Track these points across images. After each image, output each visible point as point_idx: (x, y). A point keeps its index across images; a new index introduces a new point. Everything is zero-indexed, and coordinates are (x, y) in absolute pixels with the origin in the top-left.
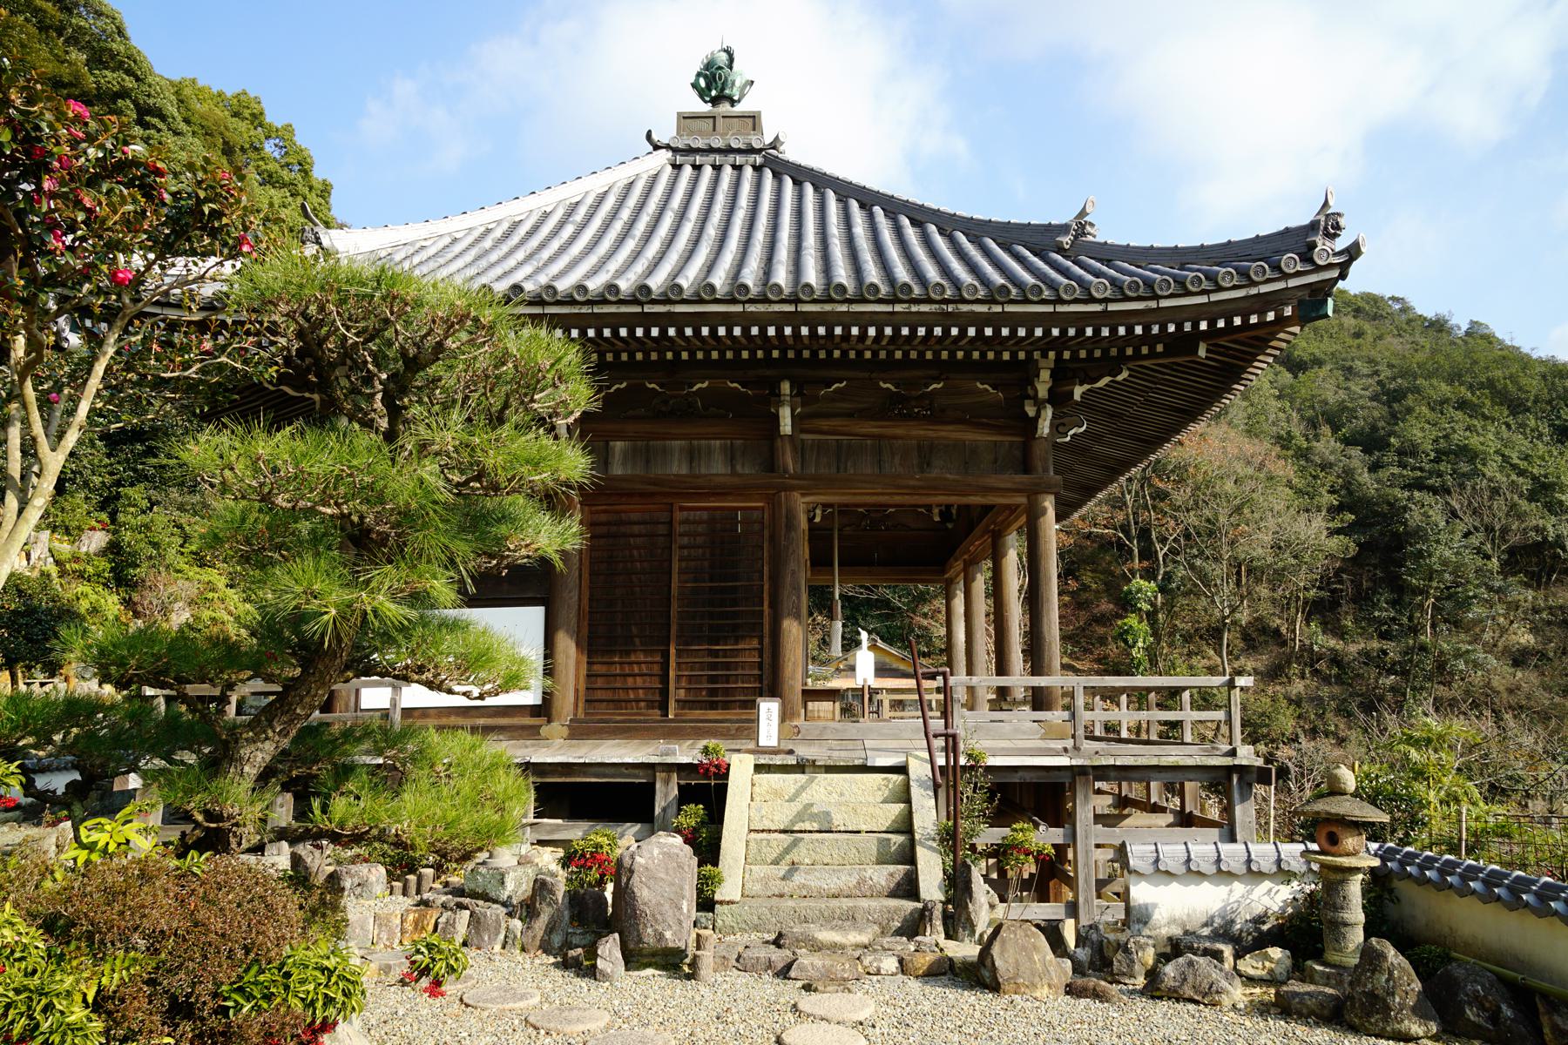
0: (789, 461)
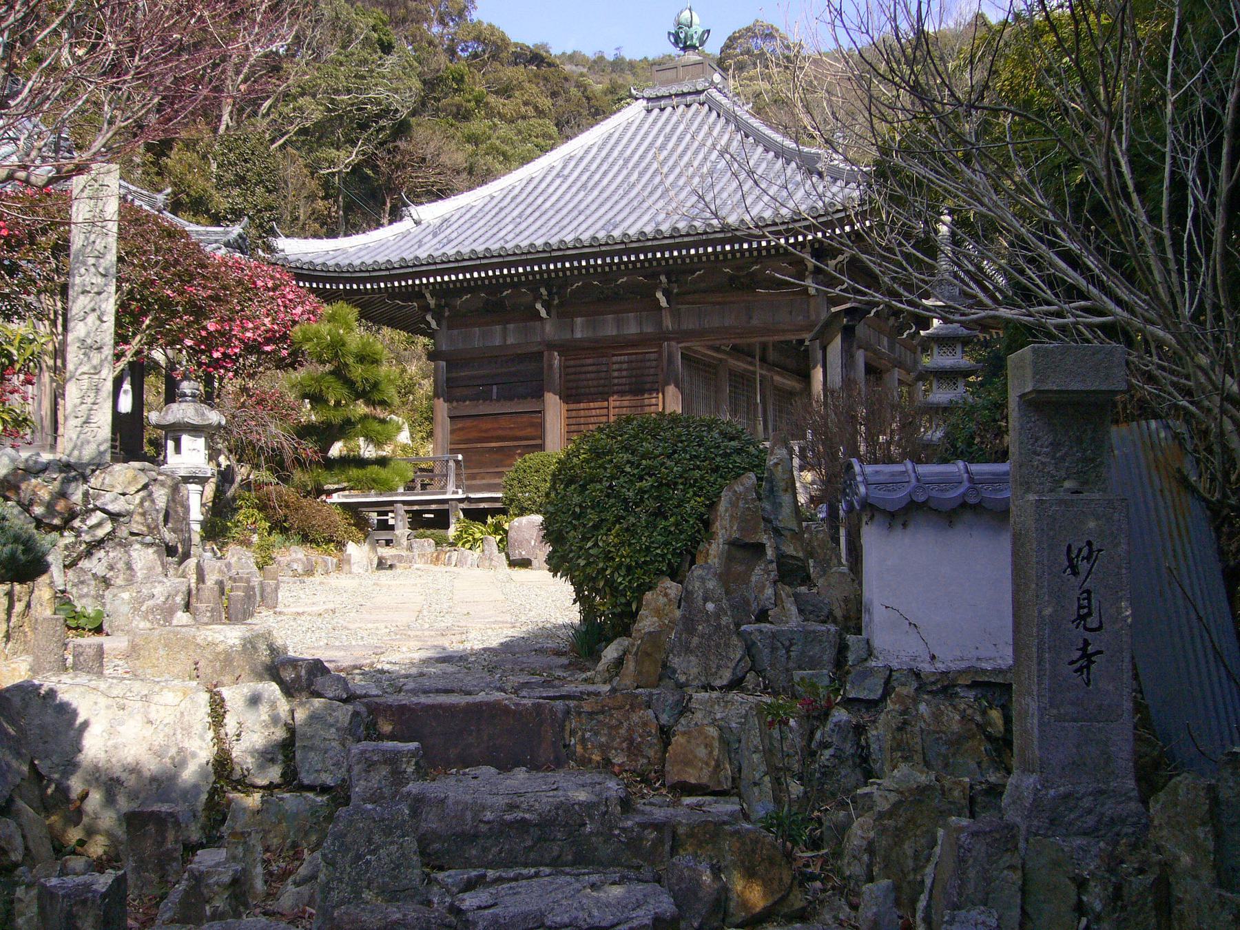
0: (668, 323)
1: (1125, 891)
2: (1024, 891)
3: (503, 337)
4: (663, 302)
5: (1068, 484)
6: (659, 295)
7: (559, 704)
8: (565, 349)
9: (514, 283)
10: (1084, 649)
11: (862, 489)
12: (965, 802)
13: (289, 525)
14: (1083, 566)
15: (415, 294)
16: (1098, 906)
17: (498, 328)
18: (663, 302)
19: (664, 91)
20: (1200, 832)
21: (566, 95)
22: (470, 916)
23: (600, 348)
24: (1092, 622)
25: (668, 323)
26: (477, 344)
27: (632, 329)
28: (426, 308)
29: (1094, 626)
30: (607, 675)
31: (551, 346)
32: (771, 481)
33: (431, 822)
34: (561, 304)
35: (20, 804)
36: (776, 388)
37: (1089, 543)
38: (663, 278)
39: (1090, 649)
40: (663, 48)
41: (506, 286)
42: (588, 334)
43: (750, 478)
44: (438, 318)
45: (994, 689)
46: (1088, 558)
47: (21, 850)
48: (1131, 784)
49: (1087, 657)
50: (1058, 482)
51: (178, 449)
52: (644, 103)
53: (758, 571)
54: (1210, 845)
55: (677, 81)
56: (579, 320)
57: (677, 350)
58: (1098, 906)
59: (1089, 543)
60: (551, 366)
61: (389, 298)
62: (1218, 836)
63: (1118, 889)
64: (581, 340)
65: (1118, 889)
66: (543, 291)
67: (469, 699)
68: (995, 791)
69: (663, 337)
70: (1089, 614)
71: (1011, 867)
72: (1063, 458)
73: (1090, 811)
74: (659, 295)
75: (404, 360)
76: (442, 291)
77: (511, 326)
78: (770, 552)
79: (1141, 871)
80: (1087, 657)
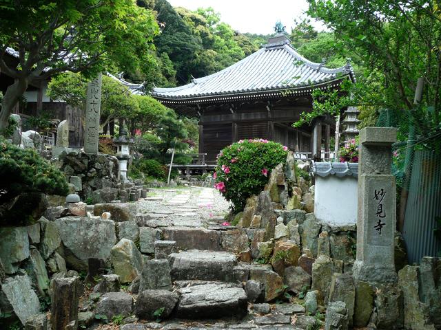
0: (270, 116)
1: (389, 300)
2: (356, 297)
3: (219, 118)
4: (268, 109)
5: (376, 171)
6: (267, 107)
7: (219, 232)
8: (240, 123)
9: (224, 103)
10: (379, 223)
11: (314, 170)
12: (341, 268)
13: (153, 173)
14: (380, 197)
15: (194, 105)
16: (380, 304)
17: (219, 116)
18: (268, 109)
19: (271, 45)
20: (414, 283)
21: (248, 46)
22: (183, 295)
23: (250, 123)
24: (382, 215)
25: (270, 116)
26: (212, 120)
27: (259, 117)
28: (198, 110)
29: (383, 215)
30: (85, 258)
31: (234, 122)
32: (288, 166)
33: (175, 265)
34: (238, 109)
35: (57, 254)
36: (302, 136)
37: (382, 190)
38: (269, 102)
39: (381, 223)
40: (272, 32)
41: (208, 105)
42: (246, 118)
43: (281, 165)
44: (201, 112)
45: (352, 233)
46: (382, 194)
47: (55, 268)
48: (392, 266)
49: (380, 225)
50: (373, 171)
51: (120, 150)
52: (265, 48)
53: (282, 193)
54: (417, 286)
55: (276, 42)
56: (243, 114)
57: (272, 124)
58: (380, 304)
59: (382, 190)
60: (234, 128)
61: (184, 107)
62: (420, 285)
63: (386, 299)
64: (245, 120)
65: (386, 299)
66: (232, 105)
67: (192, 229)
68: (350, 265)
69: (266, 121)
70: (381, 212)
71: (352, 290)
72: (375, 163)
73: (379, 274)
74: (267, 107)
75: (189, 126)
76: (202, 104)
77: (223, 115)
78: (286, 188)
79: (394, 294)
80: (380, 225)
